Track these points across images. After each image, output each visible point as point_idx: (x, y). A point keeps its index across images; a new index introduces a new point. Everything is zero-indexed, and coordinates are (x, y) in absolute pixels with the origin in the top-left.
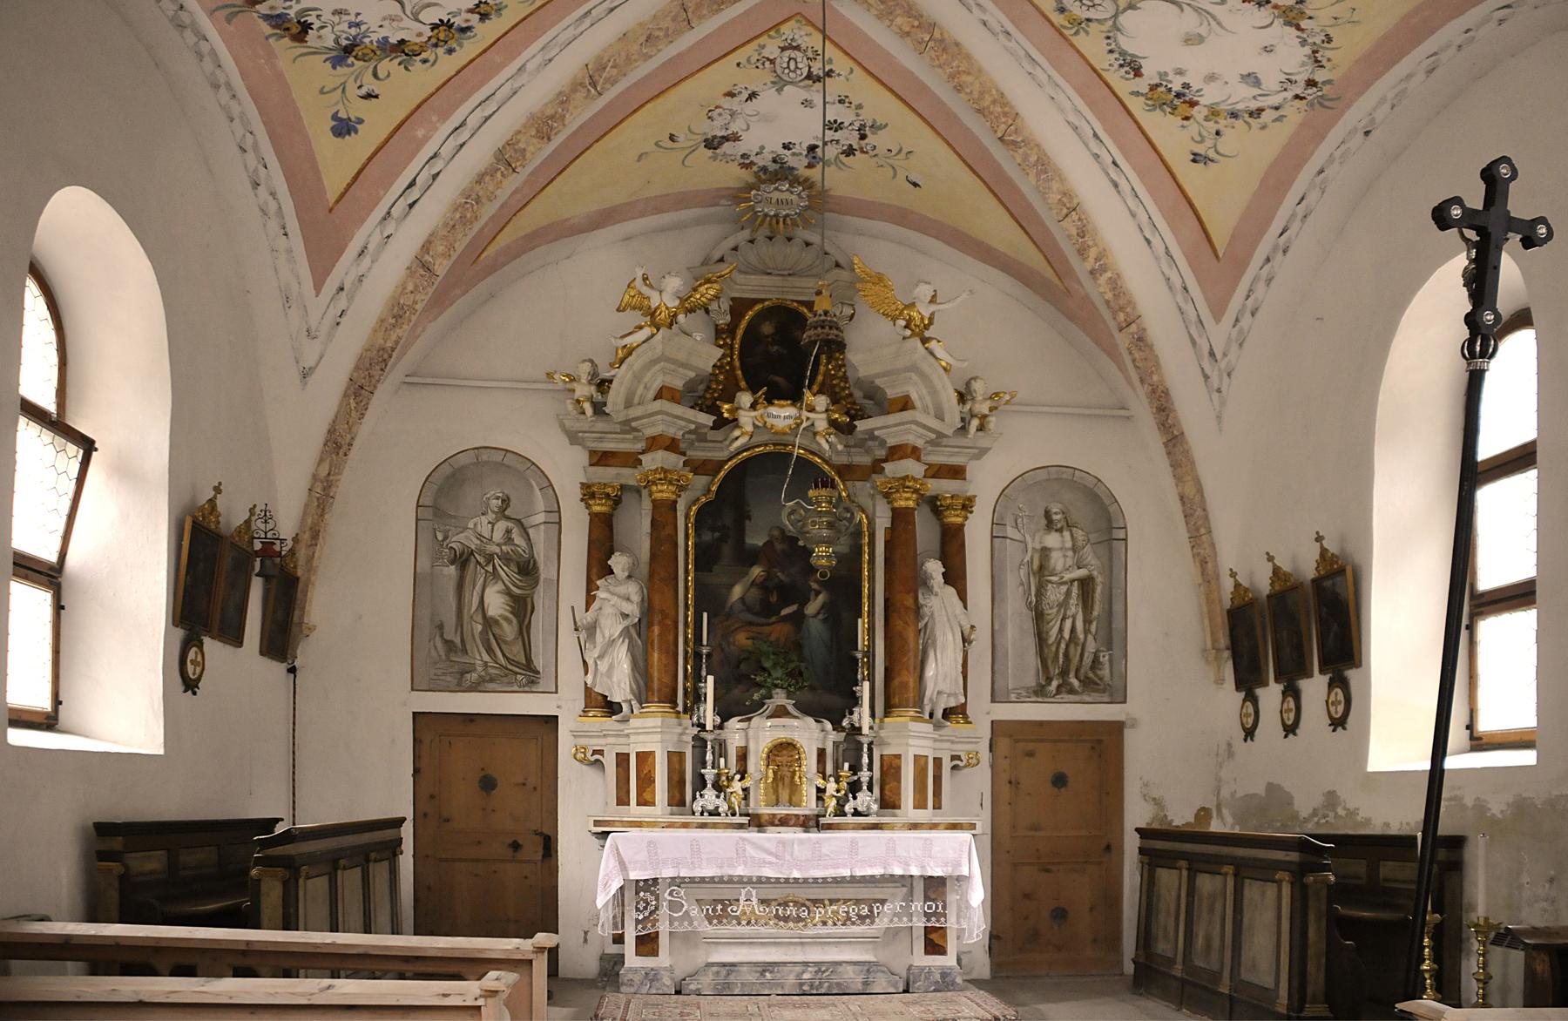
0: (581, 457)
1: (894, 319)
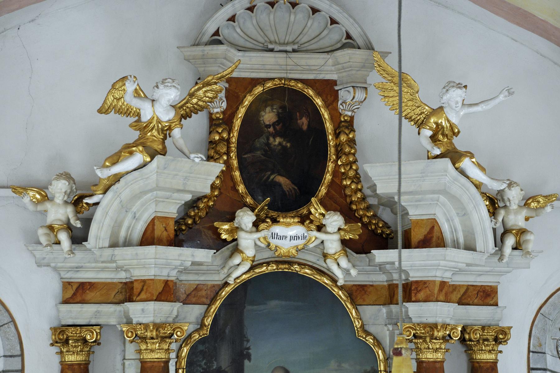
0: (51, 286)
1: (420, 125)
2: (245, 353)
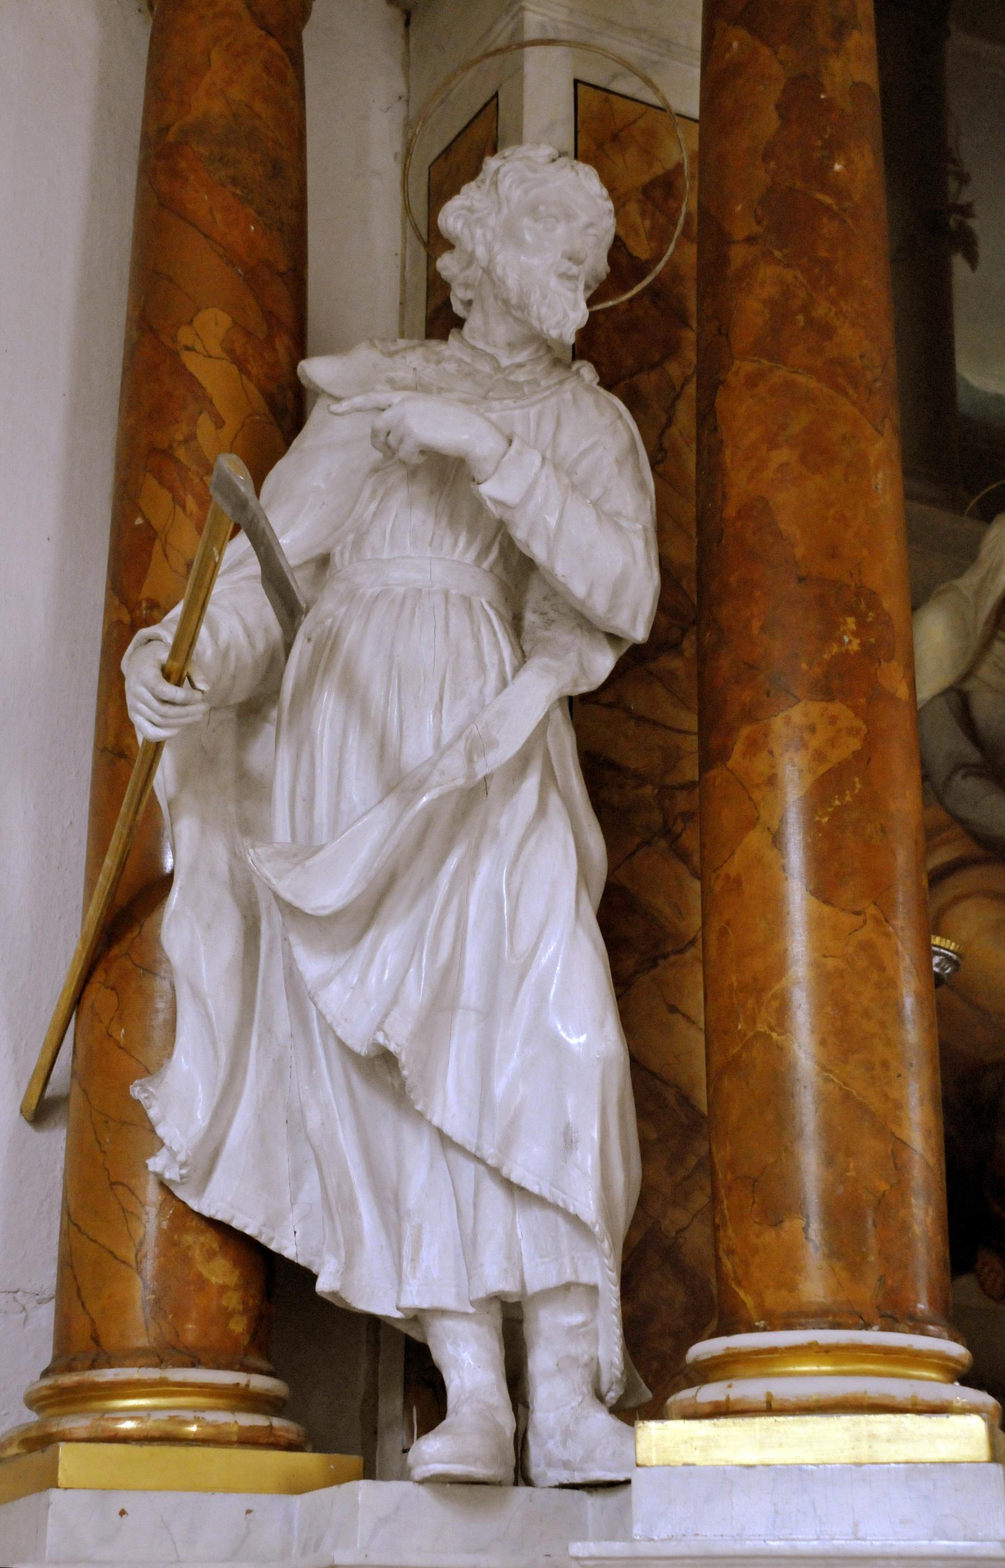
2: (952, 223)
